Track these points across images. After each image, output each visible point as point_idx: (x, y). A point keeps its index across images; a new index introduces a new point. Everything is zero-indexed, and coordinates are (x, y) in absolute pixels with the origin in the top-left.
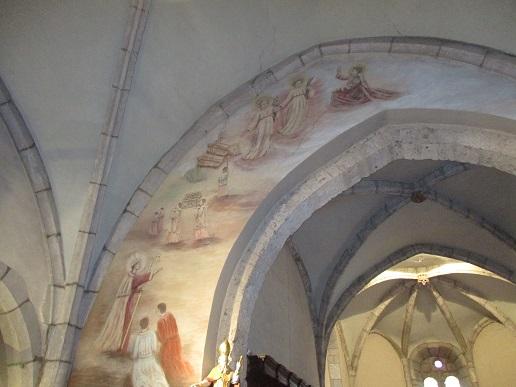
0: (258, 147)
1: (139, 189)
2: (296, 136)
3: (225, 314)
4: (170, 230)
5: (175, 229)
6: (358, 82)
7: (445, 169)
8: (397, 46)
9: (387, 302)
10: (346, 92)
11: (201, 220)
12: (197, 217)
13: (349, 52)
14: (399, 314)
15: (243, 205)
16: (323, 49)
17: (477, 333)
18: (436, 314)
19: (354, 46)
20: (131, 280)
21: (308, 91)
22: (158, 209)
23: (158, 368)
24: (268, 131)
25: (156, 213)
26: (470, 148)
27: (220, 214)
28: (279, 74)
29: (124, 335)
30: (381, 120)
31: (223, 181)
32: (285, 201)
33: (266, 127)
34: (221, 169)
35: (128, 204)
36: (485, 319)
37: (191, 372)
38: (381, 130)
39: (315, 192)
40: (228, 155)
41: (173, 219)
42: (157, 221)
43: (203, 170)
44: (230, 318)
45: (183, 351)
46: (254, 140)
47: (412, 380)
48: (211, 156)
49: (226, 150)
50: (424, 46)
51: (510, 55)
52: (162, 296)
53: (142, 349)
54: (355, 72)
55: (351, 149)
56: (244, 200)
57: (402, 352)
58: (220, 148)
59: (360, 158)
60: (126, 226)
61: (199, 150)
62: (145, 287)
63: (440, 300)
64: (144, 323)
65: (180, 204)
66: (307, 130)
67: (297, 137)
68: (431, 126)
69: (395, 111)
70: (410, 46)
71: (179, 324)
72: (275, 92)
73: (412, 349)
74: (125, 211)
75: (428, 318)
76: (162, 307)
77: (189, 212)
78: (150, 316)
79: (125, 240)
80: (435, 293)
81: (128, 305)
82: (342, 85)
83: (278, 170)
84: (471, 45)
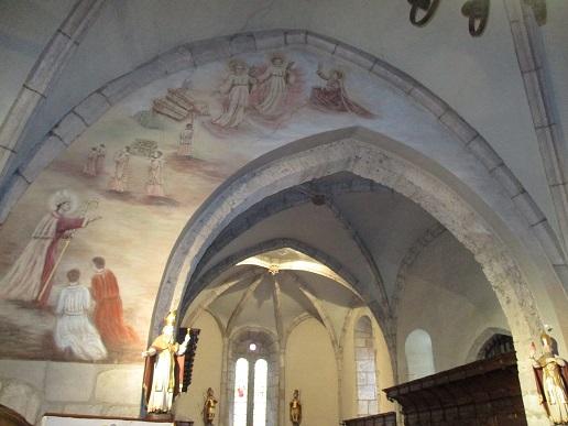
0: (231, 114)
1: (72, 111)
2: (273, 118)
3: (169, 282)
4: (113, 175)
5: (120, 176)
6: (337, 87)
7: (354, 183)
8: (380, 69)
9: (231, 284)
10: (326, 93)
11: (156, 175)
12: (150, 169)
13: (333, 53)
14: (238, 295)
15: (206, 172)
16: (310, 38)
17: (295, 325)
18: (270, 301)
19: (340, 50)
20: (56, 220)
21: (287, 75)
22: (97, 145)
23: (91, 328)
24: (241, 102)
25: (94, 149)
26: (412, 183)
27: (180, 175)
28: (260, 43)
29: (42, 285)
30: (350, 132)
31: (186, 139)
32: (245, 181)
33: (240, 96)
34: (185, 123)
35: (56, 126)
36: (306, 314)
37: (134, 336)
38: (345, 141)
39: (276, 181)
40: (194, 111)
41: (118, 163)
42: (97, 158)
43: (161, 118)
44: (173, 287)
45: (124, 315)
46: (226, 105)
47: (228, 359)
48: (170, 104)
49: (191, 104)
50: (400, 80)
51: (461, 118)
52: (98, 248)
53: (69, 304)
54: (335, 76)
55: (315, 149)
56: (211, 169)
57: (225, 332)
58: (182, 98)
59: (323, 161)
60: (49, 152)
61: (153, 91)
62: (77, 234)
63: (278, 291)
64: (74, 276)
65: (128, 149)
66: (286, 117)
67: (273, 120)
68: (386, 152)
69: (366, 129)
70: (390, 75)
71: (120, 284)
72: (253, 60)
73: (236, 331)
74: (51, 133)
75: (260, 303)
76: (99, 262)
77: (139, 161)
78: (82, 270)
79: (134, 198)
80: (276, 284)
81: (51, 248)
82: (323, 84)
83: (252, 147)
84: (468, 124)
